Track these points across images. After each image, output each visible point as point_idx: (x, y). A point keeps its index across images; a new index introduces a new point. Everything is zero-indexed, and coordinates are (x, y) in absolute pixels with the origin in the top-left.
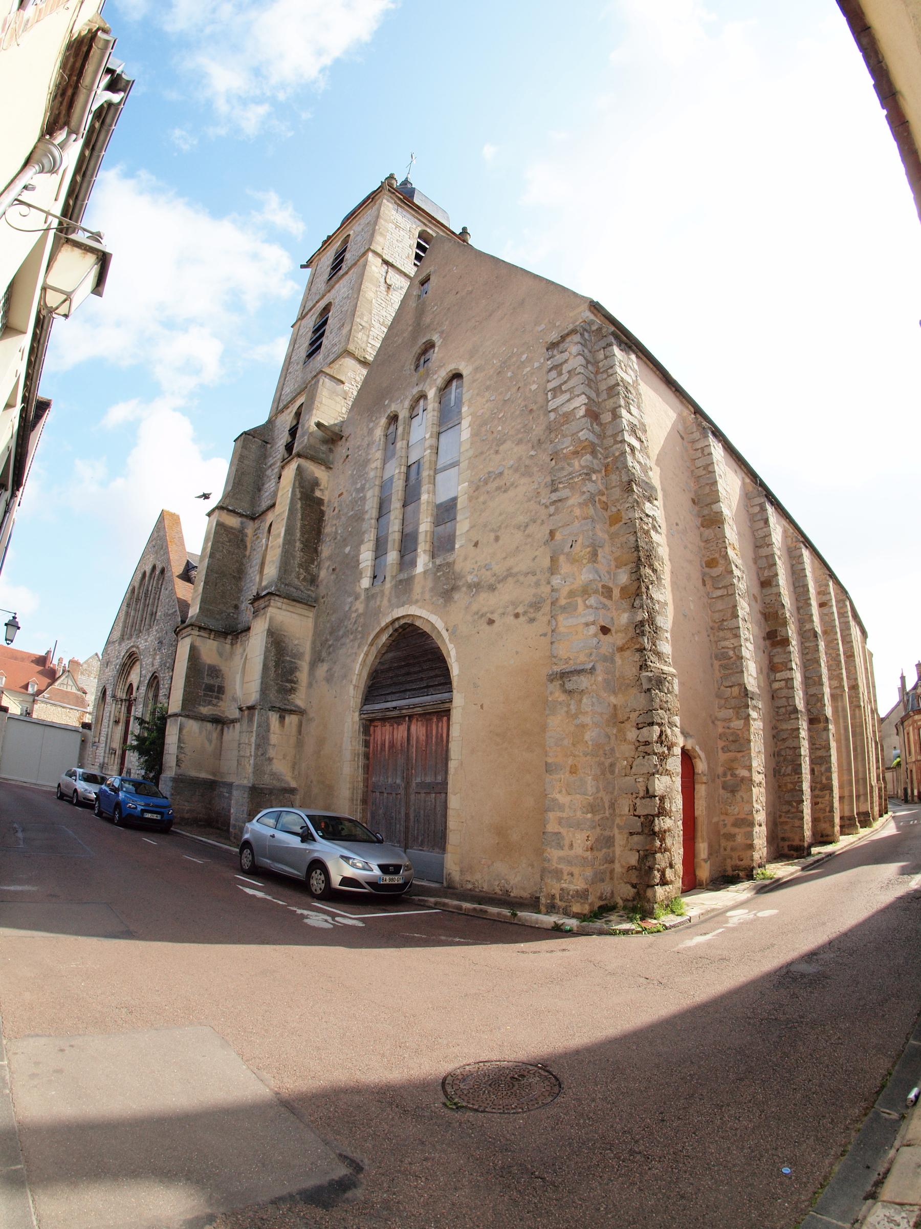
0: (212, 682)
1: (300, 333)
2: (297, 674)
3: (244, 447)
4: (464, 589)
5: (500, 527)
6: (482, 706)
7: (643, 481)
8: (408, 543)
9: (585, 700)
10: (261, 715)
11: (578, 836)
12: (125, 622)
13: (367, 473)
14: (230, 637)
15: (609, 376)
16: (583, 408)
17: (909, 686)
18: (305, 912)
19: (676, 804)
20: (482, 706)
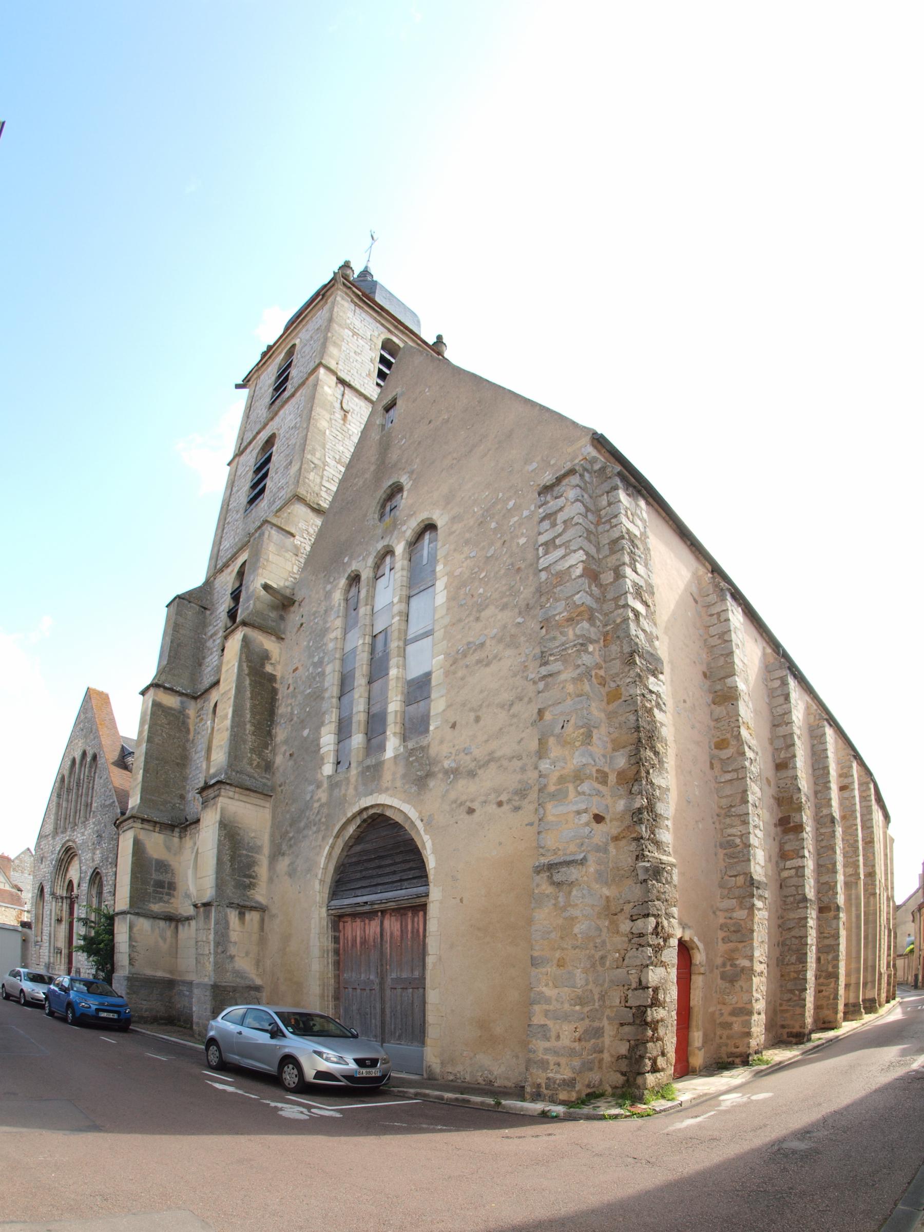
0: (161, 878)
1: (239, 473)
2: (256, 868)
3: (179, 613)
4: (440, 776)
5: (481, 706)
6: (461, 900)
7: (648, 652)
8: (375, 725)
12: (57, 814)
13: (325, 644)
14: (177, 830)
15: (612, 527)
18: (280, 1105)
19: (671, 994)
20: (461, 900)
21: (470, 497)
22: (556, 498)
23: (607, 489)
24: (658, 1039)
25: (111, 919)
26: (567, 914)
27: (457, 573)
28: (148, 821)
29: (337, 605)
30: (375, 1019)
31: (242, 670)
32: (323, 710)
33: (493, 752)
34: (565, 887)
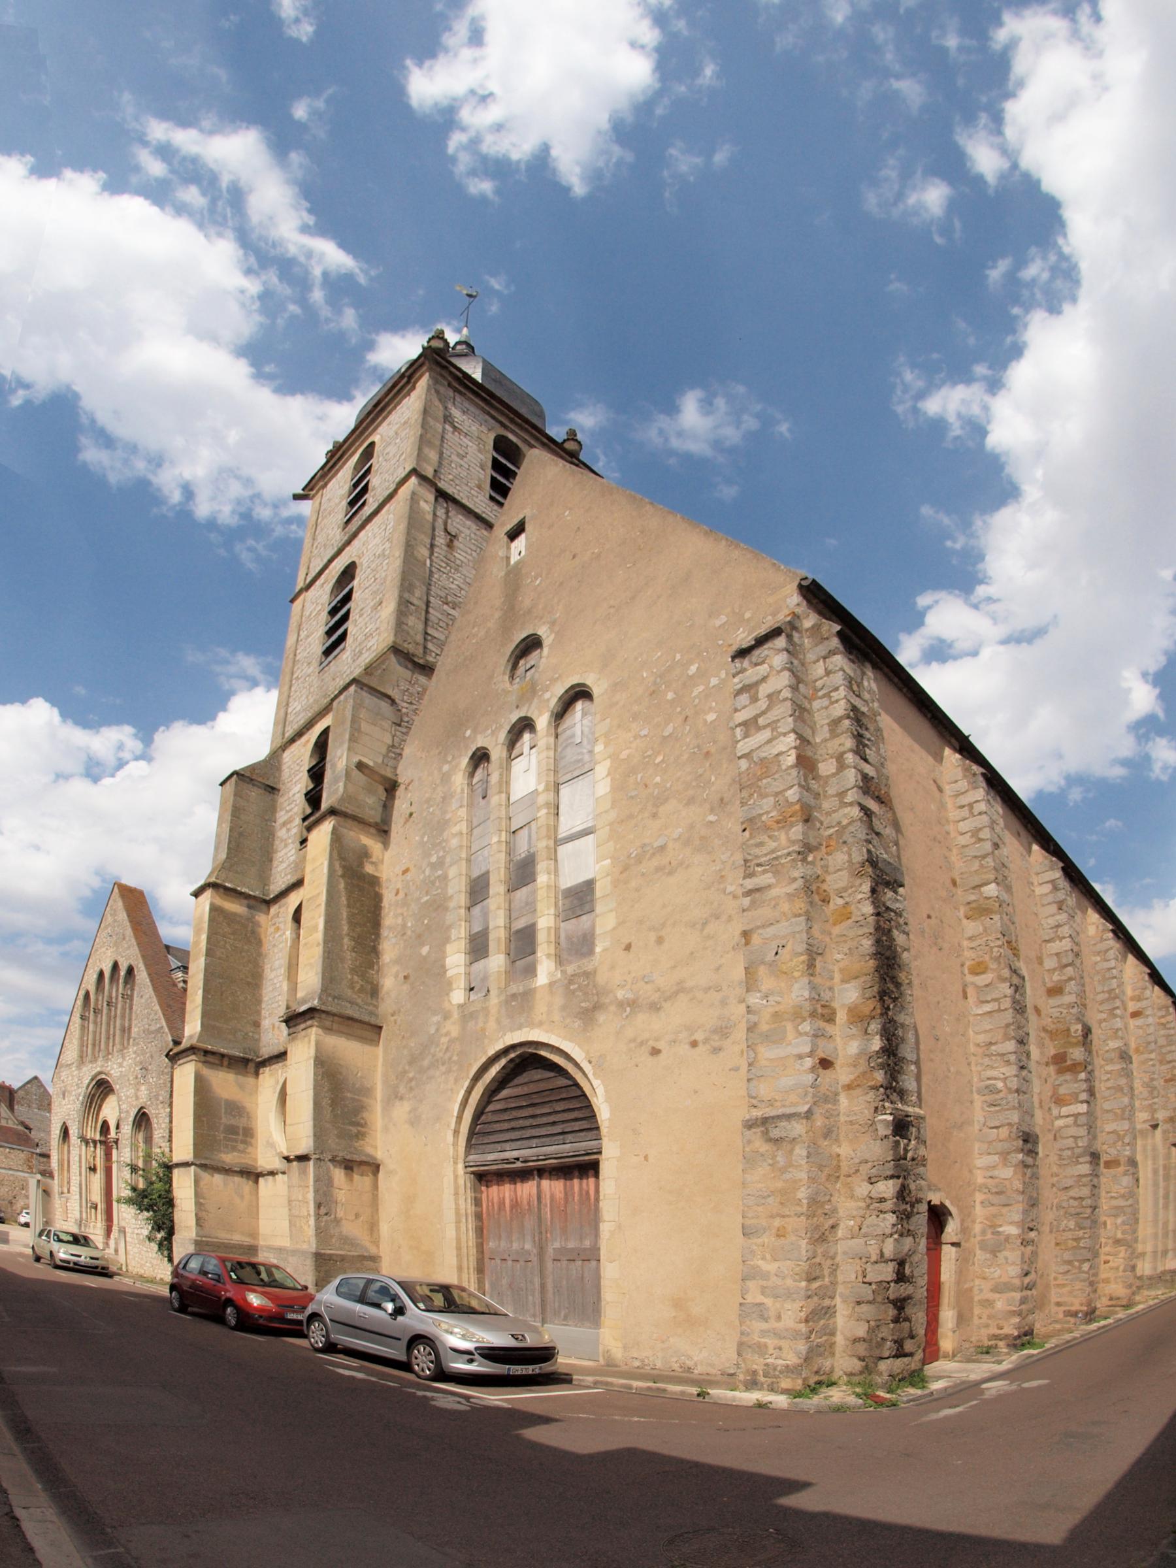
0: (233, 1122)
1: (307, 613)
2: (365, 1115)
3: (237, 794)
4: (613, 1008)
5: (663, 925)
6: (646, 1158)
8: (523, 943)
11: (788, 1306)
13: (446, 841)
15: (832, 703)
16: (793, 753)
20: (646, 1158)
21: (636, 659)
22: (756, 665)
23: (823, 653)
24: (907, 1319)
25: (168, 1168)
26: (787, 1176)
28: (213, 1053)
29: (459, 790)
30: (533, 1296)
31: (335, 871)
34: (784, 1144)
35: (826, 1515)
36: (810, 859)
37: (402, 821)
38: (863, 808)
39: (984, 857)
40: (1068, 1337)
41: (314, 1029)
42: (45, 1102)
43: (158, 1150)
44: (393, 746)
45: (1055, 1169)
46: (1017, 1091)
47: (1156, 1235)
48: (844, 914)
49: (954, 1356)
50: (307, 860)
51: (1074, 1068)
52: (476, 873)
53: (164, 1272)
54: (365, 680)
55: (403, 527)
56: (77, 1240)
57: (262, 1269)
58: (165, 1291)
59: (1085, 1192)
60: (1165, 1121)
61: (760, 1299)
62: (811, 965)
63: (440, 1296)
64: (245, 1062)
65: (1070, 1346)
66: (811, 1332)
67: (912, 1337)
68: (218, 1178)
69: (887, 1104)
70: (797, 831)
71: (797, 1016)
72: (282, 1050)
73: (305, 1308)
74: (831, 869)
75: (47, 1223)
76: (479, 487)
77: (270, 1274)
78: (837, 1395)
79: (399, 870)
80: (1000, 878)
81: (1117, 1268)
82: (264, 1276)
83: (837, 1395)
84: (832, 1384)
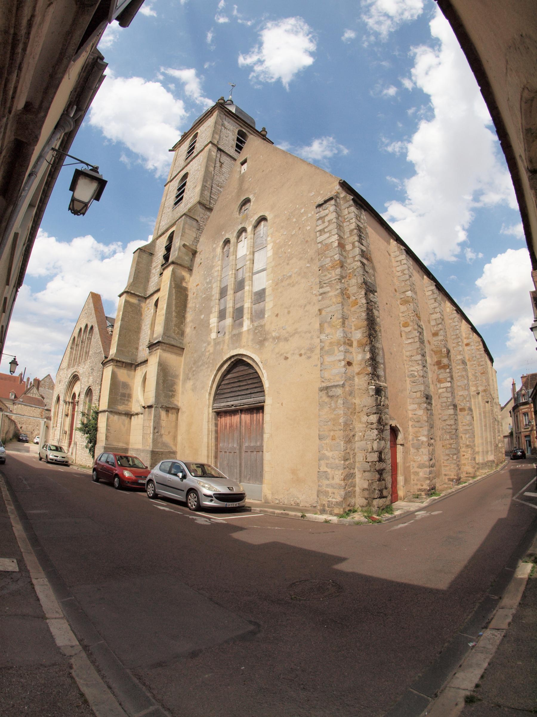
0: (124, 391)
2: (175, 387)
3: (139, 256)
4: (271, 340)
5: (290, 306)
6: (282, 404)
8: (239, 313)
9: (339, 401)
10: (155, 411)
11: (336, 472)
16: (337, 242)
17: (518, 389)
18: (194, 517)
24: (384, 480)
25: (97, 413)
26: (335, 412)
27: (277, 241)
28: (119, 361)
32: (212, 305)
33: (296, 329)
35: (353, 573)
36: (343, 281)
37: (198, 266)
38: (361, 262)
39: (406, 281)
40: (450, 491)
41: (159, 350)
42: (52, 386)
43: (94, 405)
44: (196, 238)
45: (440, 411)
46: (423, 376)
47: (483, 443)
48: (355, 303)
49: (404, 499)
50: (162, 281)
51: (445, 367)
52: (222, 286)
53: (89, 462)
54: (188, 214)
55: (205, 160)
56: (58, 449)
57: (130, 459)
58: (90, 472)
59: (452, 422)
60: (482, 391)
61: (326, 469)
62: (344, 323)
63: (200, 469)
64: (131, 365)
65: (451, 495)
66: (346, 485)
67: (386, 489)
68: (116, 417)
69: (373, 381)
70: (338, 271)
71: (339, 344)
72: (146, 359)
73: (146, 477)
74: (350, 285)
75: (46, 442)
76: (232, 147)
77: (133, 461)
78: (358, 517)
79: (195, 285)
80: (412, 289)
81: (468, 459)
82: (131, 463)
83: (358, 517)
84: (355, 511)
